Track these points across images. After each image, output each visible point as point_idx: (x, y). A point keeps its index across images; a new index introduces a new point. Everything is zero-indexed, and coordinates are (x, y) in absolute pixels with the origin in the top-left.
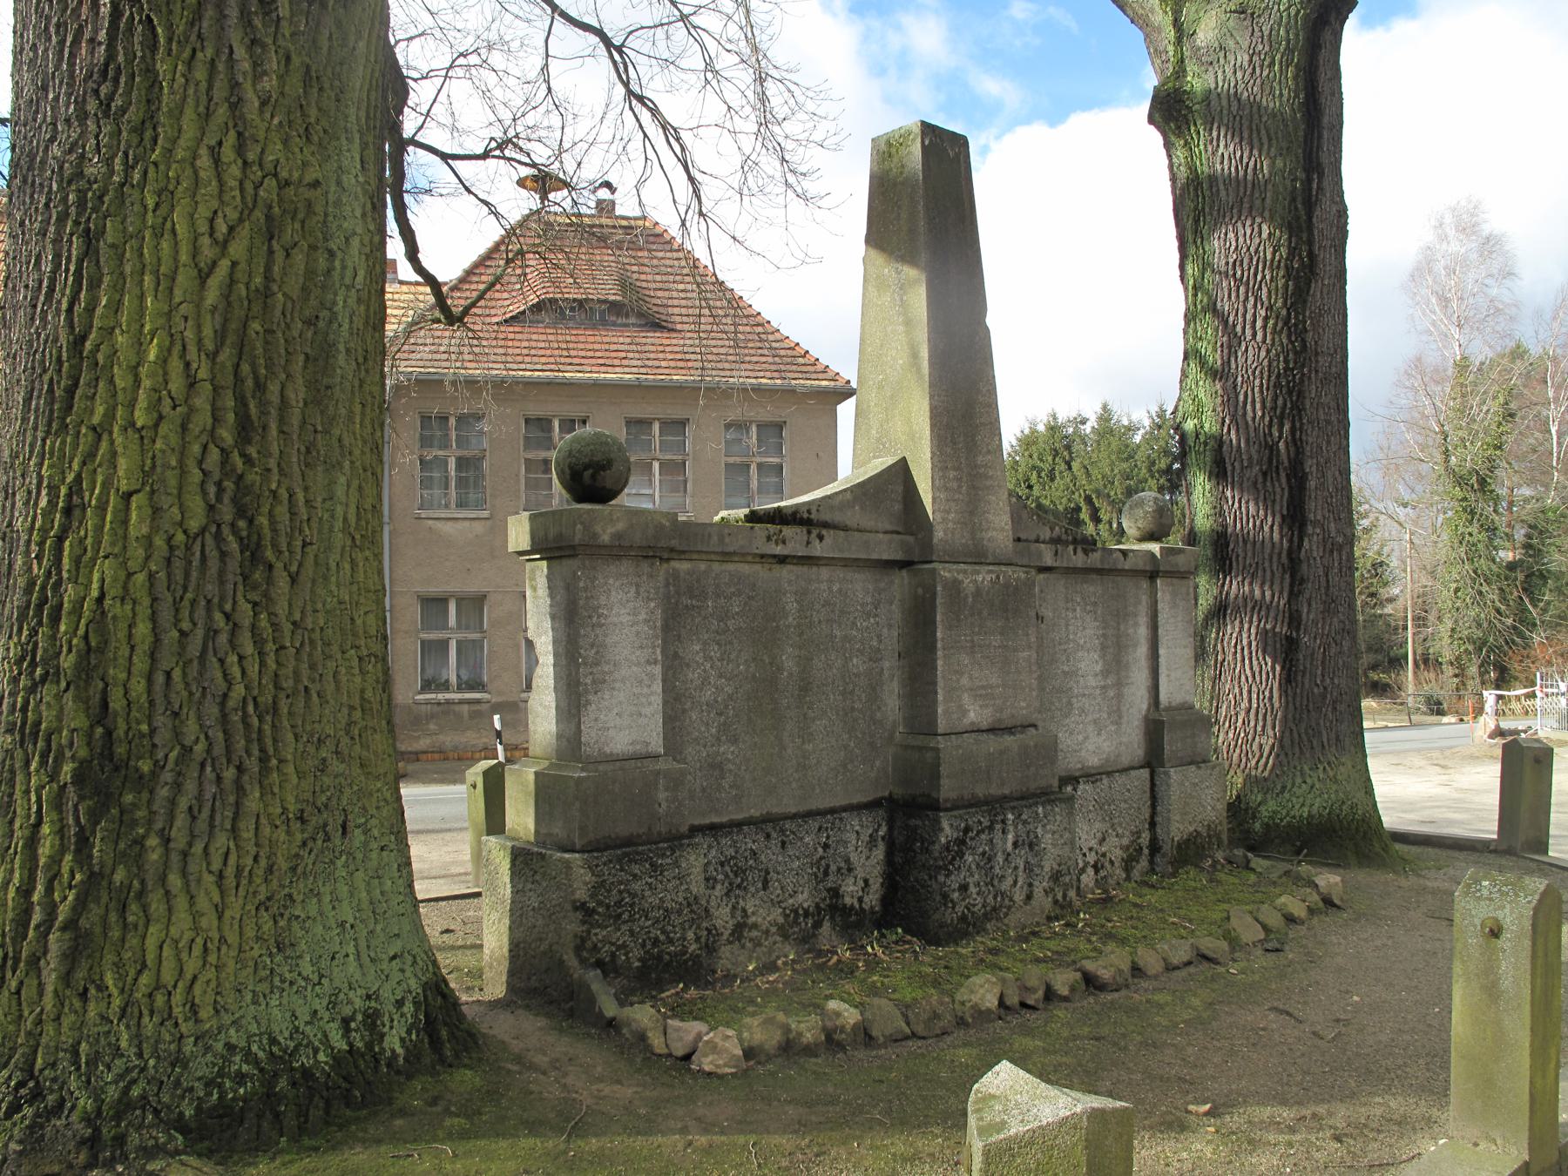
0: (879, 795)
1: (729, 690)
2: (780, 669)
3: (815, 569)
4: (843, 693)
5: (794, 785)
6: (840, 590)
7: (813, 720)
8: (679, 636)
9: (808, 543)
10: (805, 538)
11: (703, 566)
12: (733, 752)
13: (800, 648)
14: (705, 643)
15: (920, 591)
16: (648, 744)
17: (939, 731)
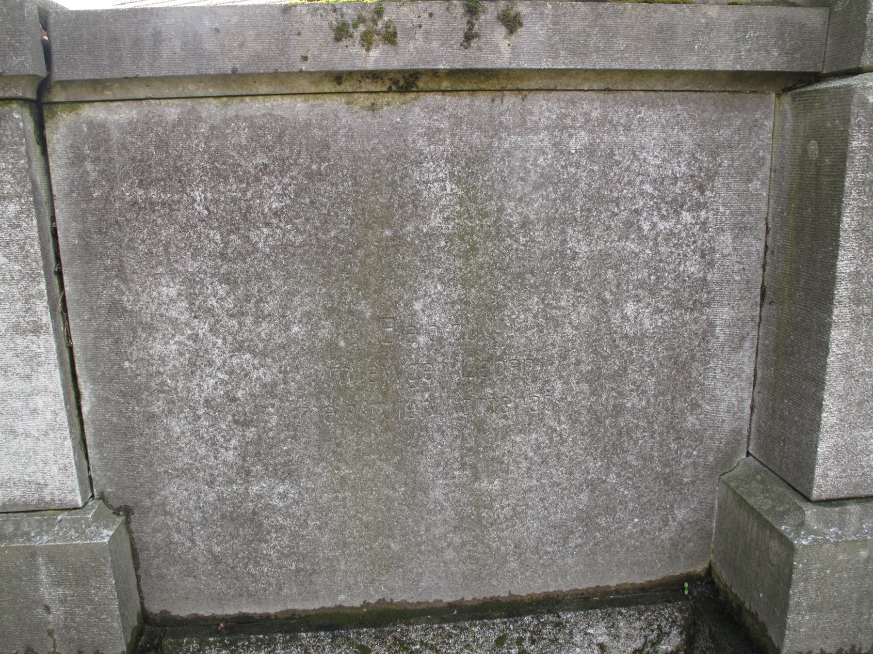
0: (679, 570)
1: (263, 375)
2: (407, 329)
3: (510, 101)
4: (594, 378)
5: (449, 555)
6: (590, 151)
7: (506, 433)
8: (121, 268)
9: (469, 37)
10: (461, 25)
11: (172, 111)
12: (283, 496)
13: (466, 283)
14: (190, 281)
15: (813, 146)
16: (40, 487)
17: (815, 494)
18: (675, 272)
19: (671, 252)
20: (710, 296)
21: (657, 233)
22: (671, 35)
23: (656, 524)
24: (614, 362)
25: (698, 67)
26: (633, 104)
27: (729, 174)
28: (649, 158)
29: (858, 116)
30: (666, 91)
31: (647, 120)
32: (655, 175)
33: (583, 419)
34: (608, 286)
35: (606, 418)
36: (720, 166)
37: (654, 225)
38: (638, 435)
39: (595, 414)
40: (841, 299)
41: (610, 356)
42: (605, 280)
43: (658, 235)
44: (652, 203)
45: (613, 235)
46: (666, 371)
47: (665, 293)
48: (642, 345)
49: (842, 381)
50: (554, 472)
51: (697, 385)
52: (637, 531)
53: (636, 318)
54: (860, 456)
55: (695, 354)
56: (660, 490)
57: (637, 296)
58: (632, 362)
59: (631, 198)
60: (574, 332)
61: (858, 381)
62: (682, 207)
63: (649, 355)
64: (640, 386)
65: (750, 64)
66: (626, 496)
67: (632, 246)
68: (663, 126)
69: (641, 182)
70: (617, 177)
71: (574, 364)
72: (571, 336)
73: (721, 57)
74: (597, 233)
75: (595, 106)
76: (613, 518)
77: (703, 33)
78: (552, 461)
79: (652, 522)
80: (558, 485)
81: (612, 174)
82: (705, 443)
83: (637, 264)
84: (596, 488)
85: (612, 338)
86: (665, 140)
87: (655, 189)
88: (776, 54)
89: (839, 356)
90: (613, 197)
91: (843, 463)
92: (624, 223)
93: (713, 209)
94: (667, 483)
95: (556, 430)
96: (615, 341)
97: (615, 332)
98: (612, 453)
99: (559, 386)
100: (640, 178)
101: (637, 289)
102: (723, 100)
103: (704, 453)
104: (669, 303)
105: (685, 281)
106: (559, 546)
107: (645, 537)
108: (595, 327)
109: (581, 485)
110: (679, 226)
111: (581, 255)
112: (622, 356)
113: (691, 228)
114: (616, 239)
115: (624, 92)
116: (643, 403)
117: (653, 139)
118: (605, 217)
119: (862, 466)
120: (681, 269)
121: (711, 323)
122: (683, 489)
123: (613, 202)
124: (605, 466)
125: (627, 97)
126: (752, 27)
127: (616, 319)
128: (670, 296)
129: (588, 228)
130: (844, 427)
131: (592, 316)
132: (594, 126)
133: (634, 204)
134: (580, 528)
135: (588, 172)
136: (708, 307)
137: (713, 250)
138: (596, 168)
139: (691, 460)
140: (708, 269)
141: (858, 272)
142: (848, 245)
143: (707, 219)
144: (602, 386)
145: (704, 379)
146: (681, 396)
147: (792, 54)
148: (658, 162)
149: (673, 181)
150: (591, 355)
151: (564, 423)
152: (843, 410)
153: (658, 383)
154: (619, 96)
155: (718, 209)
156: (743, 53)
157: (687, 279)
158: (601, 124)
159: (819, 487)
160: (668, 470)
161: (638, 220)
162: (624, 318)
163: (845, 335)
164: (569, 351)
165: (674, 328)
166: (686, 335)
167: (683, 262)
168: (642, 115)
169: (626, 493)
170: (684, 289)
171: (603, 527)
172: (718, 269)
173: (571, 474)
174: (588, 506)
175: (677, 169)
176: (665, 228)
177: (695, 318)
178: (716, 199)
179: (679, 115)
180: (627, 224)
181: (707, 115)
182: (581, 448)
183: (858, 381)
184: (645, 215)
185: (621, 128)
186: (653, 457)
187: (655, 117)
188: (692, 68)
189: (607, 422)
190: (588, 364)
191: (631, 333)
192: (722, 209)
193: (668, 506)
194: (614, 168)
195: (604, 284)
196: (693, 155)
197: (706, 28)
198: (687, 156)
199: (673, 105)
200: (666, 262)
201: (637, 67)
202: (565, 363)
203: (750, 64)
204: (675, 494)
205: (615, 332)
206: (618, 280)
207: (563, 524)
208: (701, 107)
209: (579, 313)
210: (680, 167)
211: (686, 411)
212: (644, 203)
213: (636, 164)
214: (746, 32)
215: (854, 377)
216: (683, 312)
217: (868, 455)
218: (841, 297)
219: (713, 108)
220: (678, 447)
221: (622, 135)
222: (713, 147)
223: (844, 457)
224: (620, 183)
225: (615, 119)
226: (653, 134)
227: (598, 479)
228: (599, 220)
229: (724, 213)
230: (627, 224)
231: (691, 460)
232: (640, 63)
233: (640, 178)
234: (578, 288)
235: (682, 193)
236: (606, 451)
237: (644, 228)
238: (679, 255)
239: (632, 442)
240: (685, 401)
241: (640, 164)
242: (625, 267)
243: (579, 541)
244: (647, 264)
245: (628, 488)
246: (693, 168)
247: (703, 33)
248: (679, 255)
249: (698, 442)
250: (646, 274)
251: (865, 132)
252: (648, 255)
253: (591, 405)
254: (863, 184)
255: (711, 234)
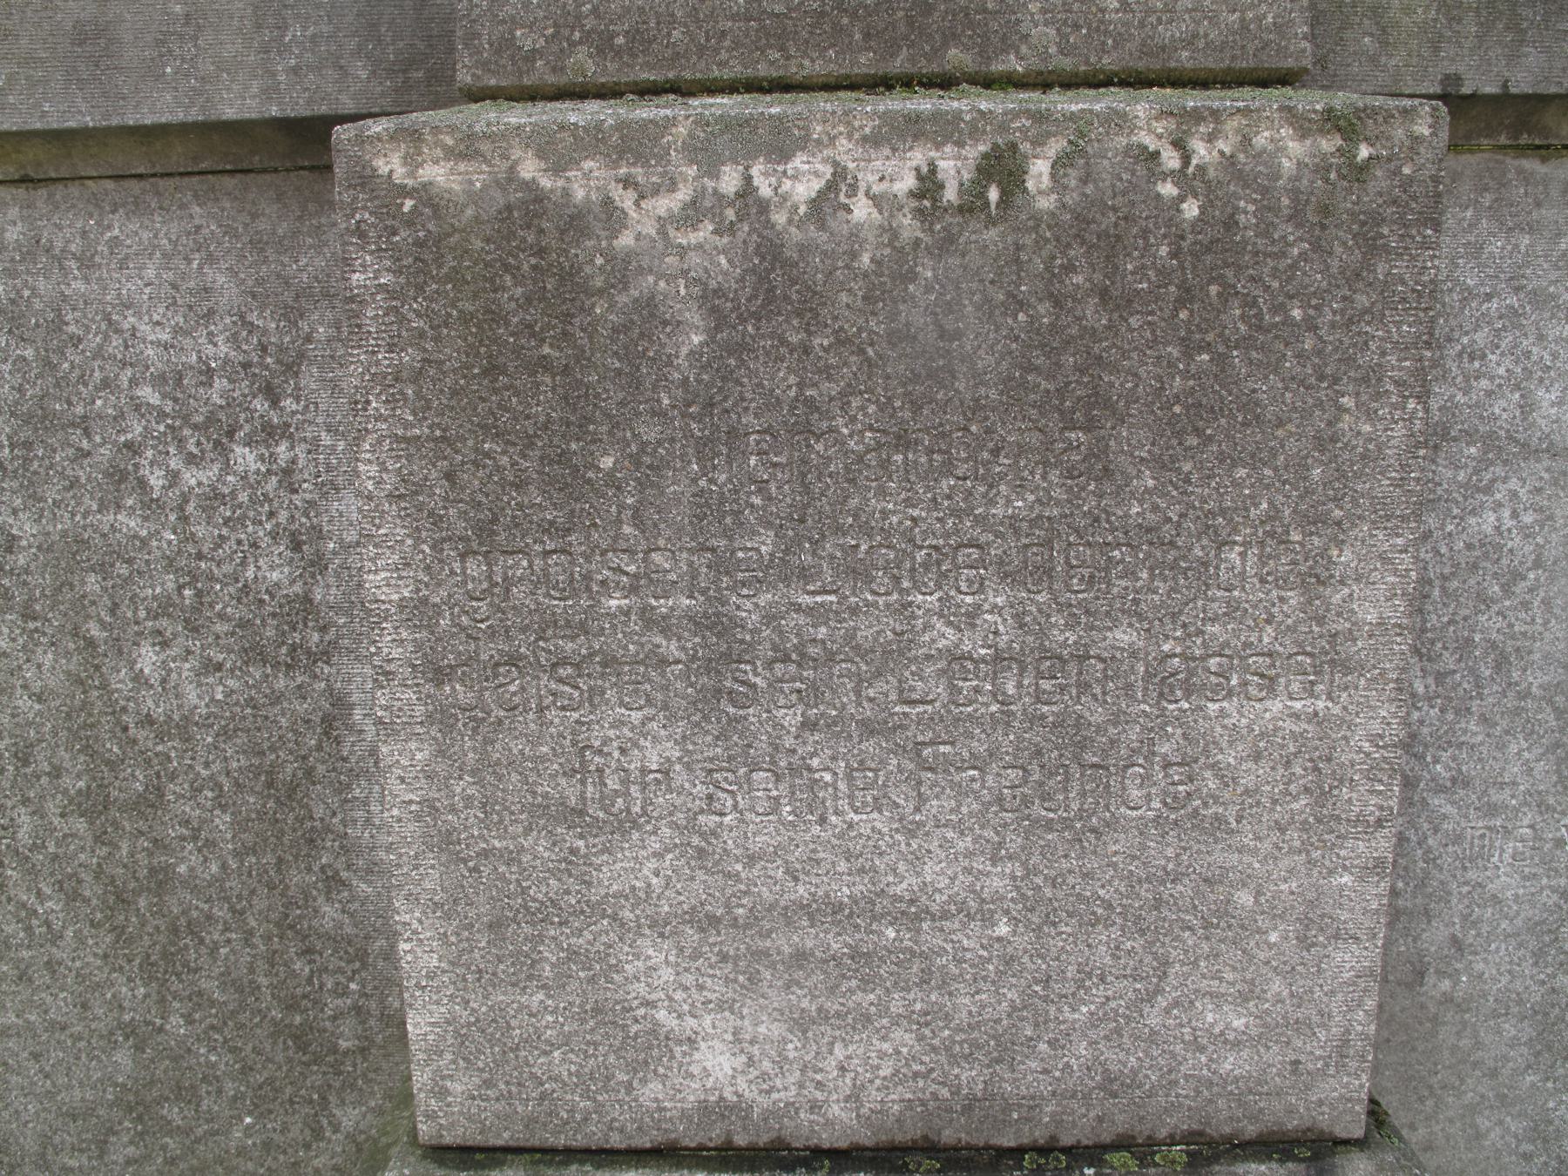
4: (93, 804)
18: (237, 581)
19: (220, 536)
20: (327, 638)
21: (183, 494)
22: (107, 48)
23: (295, 1132)
24: (133, 775)
25: (180, 116)
26: (91, 208)
27: (332, 357)
28: (143, 328)
29: (355, 210)
30: (163, 175)
31: (129, 242)
32: (160, 365)
33: (87, 893)
34: (92, 610)
35: (137, 893)
36: (308, 339)
37: (174, 478)
38: (216, 937)
39: (113, 882)
40: (392, 667)
41: (123, 761)
42: (84, 596)
43: (185, 499)
44: (162, 428)
45: (87, 500)
46: (252, 800)
47: (221, 628)
48: (187, 740)
49: (433, 867)
50: (49, 999)
51: (331, 836)
52: (254, 1144)
53: (164, 681)
54: (523, 1053)
55: (313, 768)
56: (290, 1060)
57: (160, 633)
58: (173, 777)
59: (115, 418)
60: (37, 707)
61: (476, 869)
62: (231, 434)
63: (207, 765)
64: (199, 830)
65: (301, 101)
66: (214, 1066)
67: (132, 524)
68: (164, 255)
69: (130, 381)
70: (77, 373)
71: (49, 774)
72: (31, 716)
73: (229, 90)
74: (51, 494)
75: (9, 217)
76: (196, 1111)
77: (181, 37)
78: (41, 978)
79: (285, 1129)
80: (63, 1029)
81: (66, 365)
82: (375, 967)
83: (147, 562)
84: (144, 1041)
85: (118, 722)
86: (175, 287)
87: (164, 396)
88: (364, 74)
89: (413, 807)
90: (74, 415)
91: (481, 1064)
92: (107, 474)
93: (305, 440)
94: (303, 1047)
95: (35, 911)
96: (125, 729)
97: (124, 709)
98: (166, 972)
99: (24, 819)
100: (129, 372)
101: (156, 618)
102: (298, 189)
103: (375, 988)
104: (233, 651)
105: (262, 601)
106: (90, 1158)
107: (275, 1159)
108: (79, 696)
109: (112, 1033)
110: (230, 478)
111: (24, 543)
112: (148, 761)
113: (259, 483)
114: (95, 507)
115: (69, 183)
116: (214, 868)
117: (146, 285)
118: (63, 459)
119: (533, 1076)
120: (250, 574)
121: (339, 699)
122: (343, 1063)
123: (73, 425)
124: (154, 997)
125: (77, 194)
126: (298, 16)
127: (121, 681)
128: (233, 634)
129: (31, 483)
130: (465, 980)
131: (68, 673)
132: (13, 260)
133: (125, 432)
134: (127, 1124)
135: (14, 362)
136: (327, 663)
137: (318, 533)
138: (29, 353)
139: (349, 1001)
140: (313, 576)
141: (424, 601)
142: (382, 531)
143: (294, 461)
144: (115, 824)
145: (344, 822)
146: (296, 857)
147: (404, 71)
148: (165, 337)
149: (203, 378)
150: (82, 758)
151: (51, 898)
152: (453, 939)
153: (240, 825)
154: (59, 191)
155: (317, 439)
156: (282, 78)
157: (266, 597)
158: (29, 256)
159: (431, 1116)
160: (298, 1019)
161: (136, 466)
162: (139, 678)
163: (419, 756)
164: (32, 745)
165: (254, 707)
166: (283, 722)
167: (251, 560)
168: (116, 232)
169: (213, 1059)
170: (263, 620)
171: (178, 1127)
172: (338, 575)
173: (85, 1006)
174: (136, 1080)
175: (210, 350)
176: (200, 484)
177: (299, 687)
178: (309, 416)
179: (198, 228)
180: (112, 475)
181: (263, 225)
182: (95, 955)
183: (476, 869)
184: (149, 453)
185: (73, 264)
186: (259, 987)
187: (145, 235)
188: (163, 120)
189: (142, 903)
190: (79, 777)
191: (159, 712)
192: (326, 439)
193: (316, 1097)
194: (69, 351)
195: (82, 604)
196: (242, 317)
197: (187, 24)
198: (228, 321)
199: (182, 206)
200: (212, 559)
201: (38, 126)
202: (28, 770)
203: (301, 101)
204: (324, 1073)
205: (124, 709)
206: (111, 597)
207: (90, 1111)
208: (248, 207)
209: (39, 666)
210: (215, 345)
211: (314, 893)
212: (145, 428)
213: (116, 341)
214: (283, 28)
215: (465, 861)
216: (269, 671)
217: (545, 1053)
218: (389, 661)
219: (275, 207)
220: (312, 971)
221: (75, 278)
222: (288, 297)
223: (480, 1052)
224: (86, 385)
225: (59, 244)
226: (144, 273)
227: (147, 1023)
228: (51, 466)
229: (333, 448)
230: (112, 475)
231: (349, 1001)
232: (44, 114)
233: (129, 372)
234: (28, 615)
235: (228, 404)
236: (152, 965)
237: (152, 482)
238: (239, 542)
239: (203, 950)
240: (309, 870)
241: (125, 341)
242: (123, 570)
243: (131, 1150)
244: (170, 564)
245: (215, 1049)
246: (245, 347)
247: (181, 37)
248: (239, 542)
249: (357, 965)
250: (171, 585)
251: (380, 250)
252: (170, 542)
253: (99, 865)
254: (396, 380)
255: (308, 496)
